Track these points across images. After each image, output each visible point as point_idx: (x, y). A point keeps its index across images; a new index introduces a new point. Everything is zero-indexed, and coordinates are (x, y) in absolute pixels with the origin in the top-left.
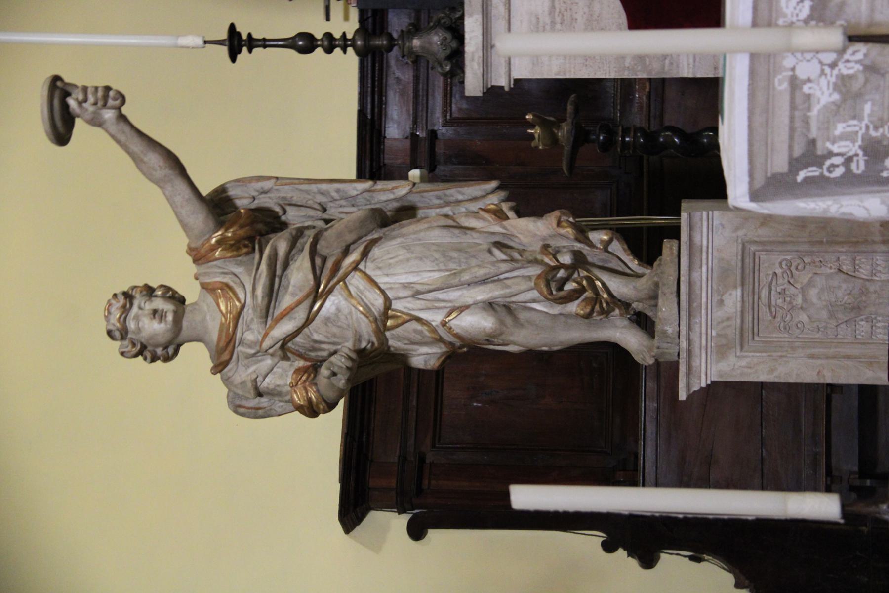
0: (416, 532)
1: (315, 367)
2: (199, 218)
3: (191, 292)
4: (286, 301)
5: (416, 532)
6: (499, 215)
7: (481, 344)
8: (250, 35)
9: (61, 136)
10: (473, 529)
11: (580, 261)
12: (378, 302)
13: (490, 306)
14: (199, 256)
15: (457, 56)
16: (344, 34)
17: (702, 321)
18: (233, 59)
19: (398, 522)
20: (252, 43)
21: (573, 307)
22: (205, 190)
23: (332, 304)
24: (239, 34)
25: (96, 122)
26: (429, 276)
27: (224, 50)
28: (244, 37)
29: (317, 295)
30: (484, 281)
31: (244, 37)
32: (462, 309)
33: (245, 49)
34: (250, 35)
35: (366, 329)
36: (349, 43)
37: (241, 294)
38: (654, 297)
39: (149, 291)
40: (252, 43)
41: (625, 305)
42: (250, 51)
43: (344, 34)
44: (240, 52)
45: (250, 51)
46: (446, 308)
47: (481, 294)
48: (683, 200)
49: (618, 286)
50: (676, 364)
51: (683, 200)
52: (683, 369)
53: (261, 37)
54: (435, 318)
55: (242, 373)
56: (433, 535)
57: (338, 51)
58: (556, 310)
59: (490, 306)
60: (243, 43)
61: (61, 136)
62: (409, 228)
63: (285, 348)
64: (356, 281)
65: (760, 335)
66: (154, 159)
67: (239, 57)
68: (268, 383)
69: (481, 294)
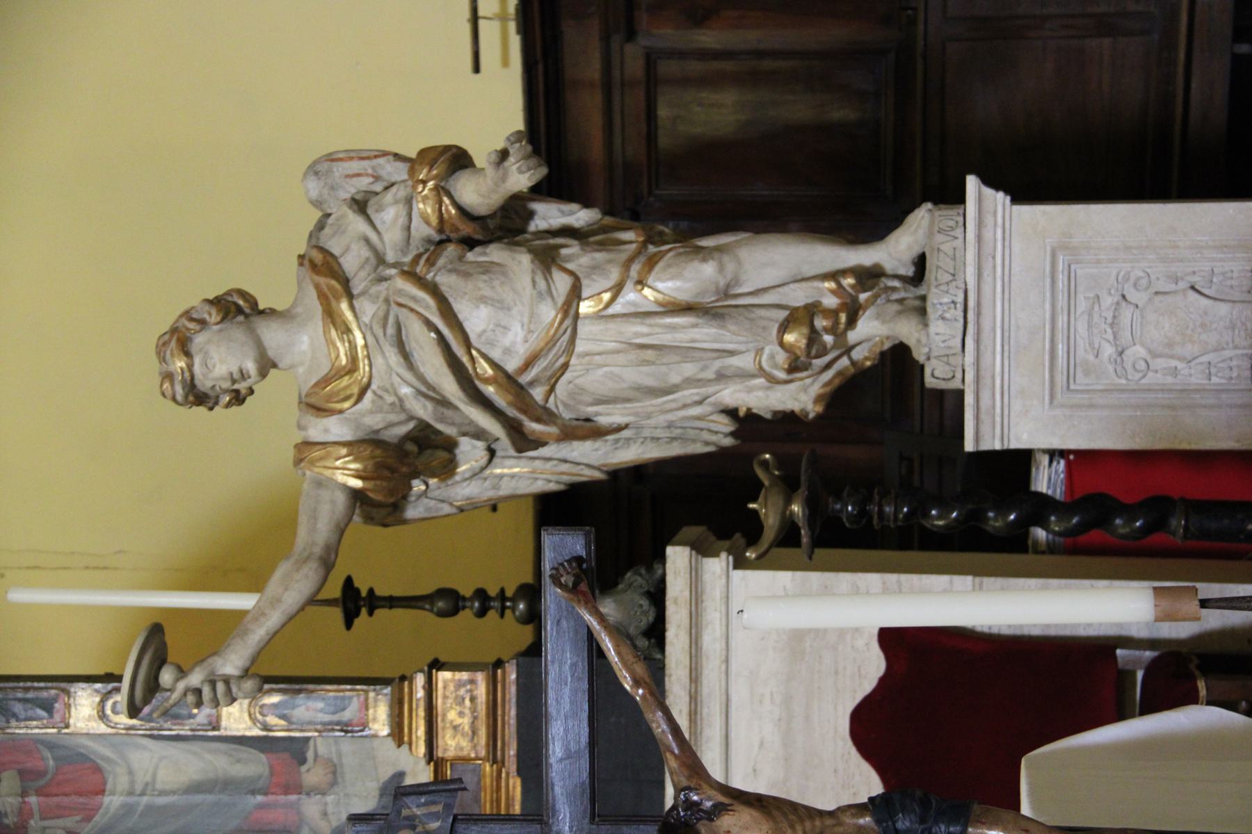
7: (743, 239)
8: (371, 591)
10: (705, 768)
16: (502, 591)
18: (349, 624)
20: (374, 602)
24: (358, 591)
27: (337, 614)
28: (364, 593)
31: (364, 593)
33: (364, 611)
34: (371, 591)
36: (508, 604)
37: (420, 679)
40: (374, 602)
42: (371, 613)
43: (502, 591)
44: (357, 614)
45: (371, 613)
46: (659, 821)
48: (1033, 488)
50: (960, 394)
51: (1033, 488)
52: (969, 400)
53: (386, 594)
57: (492, 615)
60: (362, 603)
65: (1078, 381)
67: (357, 622)
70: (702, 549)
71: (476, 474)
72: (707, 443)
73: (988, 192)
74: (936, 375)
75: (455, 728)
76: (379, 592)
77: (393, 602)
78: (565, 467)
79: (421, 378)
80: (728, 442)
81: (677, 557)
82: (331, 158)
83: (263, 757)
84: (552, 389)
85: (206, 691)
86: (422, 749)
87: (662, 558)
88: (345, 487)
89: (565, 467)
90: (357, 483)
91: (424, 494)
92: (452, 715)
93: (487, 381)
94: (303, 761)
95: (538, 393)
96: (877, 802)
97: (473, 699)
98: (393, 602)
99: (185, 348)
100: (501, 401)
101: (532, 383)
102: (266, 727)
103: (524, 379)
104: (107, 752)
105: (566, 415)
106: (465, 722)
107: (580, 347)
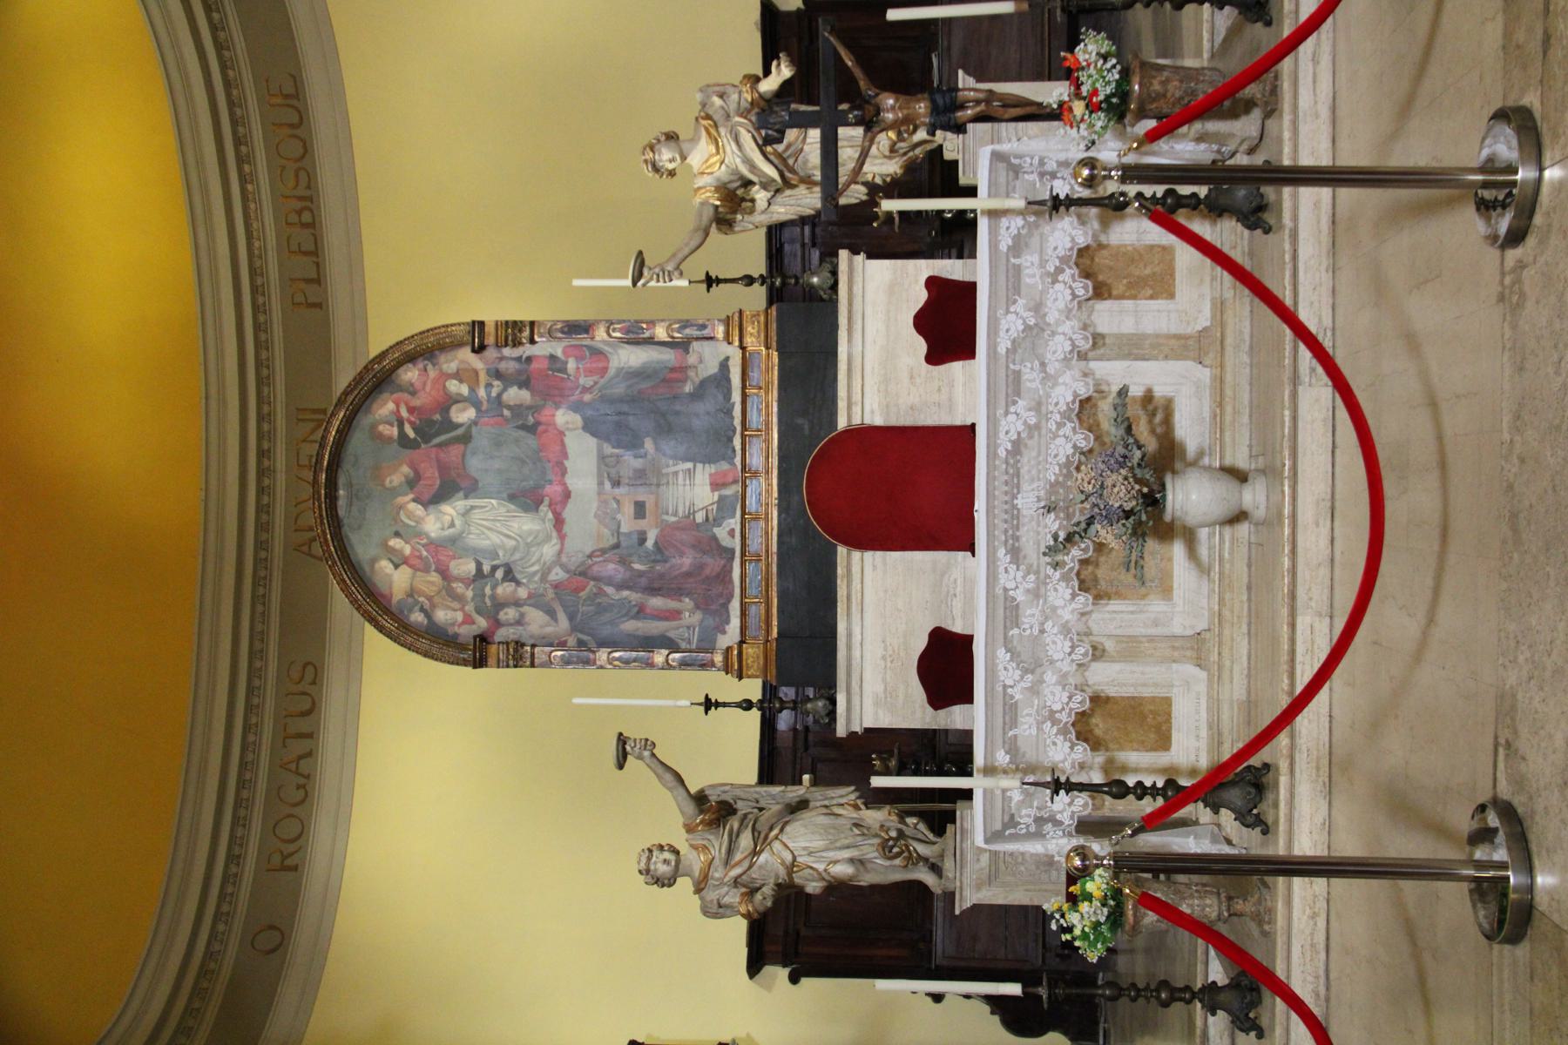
0: (794, 979)
1: (752, 892)
2: (690, 808)
3: (684, 848)
4: (738, 856)
5: (794, 979)
6: (856, 807)
9: (621, 766)
11: (901, 834)
12: (788, 858)
13: (851, 861)
14: (690, 829)
15: (832, 714)
17: (968, 870)
19: (782, 973)
21: (897, 862)
22: (693, 790)
23: (763, 858)
25: (640, 757)
26: (818, 843)
29: (755, 853)
30: (848, 847)
32: (836, 862)
33: (714, 285)
35: (782, 872)
38: (942, 856)
39: (661, 848)
41: (926, 860)
47: (847, 854)
49: (922, 849)
54: (821, 867)
55: (712, 895)
56: (805, 981)
58: (888, 863)
59: (851, 861)
61: (621, 762)
62: (805, 815)
63: (736, 882)
64: (777, 845)
66: (668, 777)
68: (727, 900)
69: (847, 854)
70: (855, 251)
71: (763, 212)
72: (857, 198)
73: (967, 77)
74: (921, 346)
75: (751, 334)
76: (720, 277)
77: (726, 281)
78: (799, 209)
79: (744, 156)
80: (864, 198)
81: (844, 254)
82: (708, 86)
83: (672, 351)
84: (796, 160)
85: (661, 274)
86: (737, 343)
87: (837, 255)
88: (713, 205)
89: (799, 209)
90: (718, 203)
91: (742, 220)
92: (750, 329)
93: (771, 154)
94: (688, 353)
95: (791, 162)
96: (954, 252)
97: (758, 322)
98: (726, 281)
99: (652, 148)
100: (776, 161)
101: (788, 157)
102: (673, 337)
103: (785, 156)
104: (610, 350)
105: (802, 174)
106: (755, 331)
107: (808, 140)
